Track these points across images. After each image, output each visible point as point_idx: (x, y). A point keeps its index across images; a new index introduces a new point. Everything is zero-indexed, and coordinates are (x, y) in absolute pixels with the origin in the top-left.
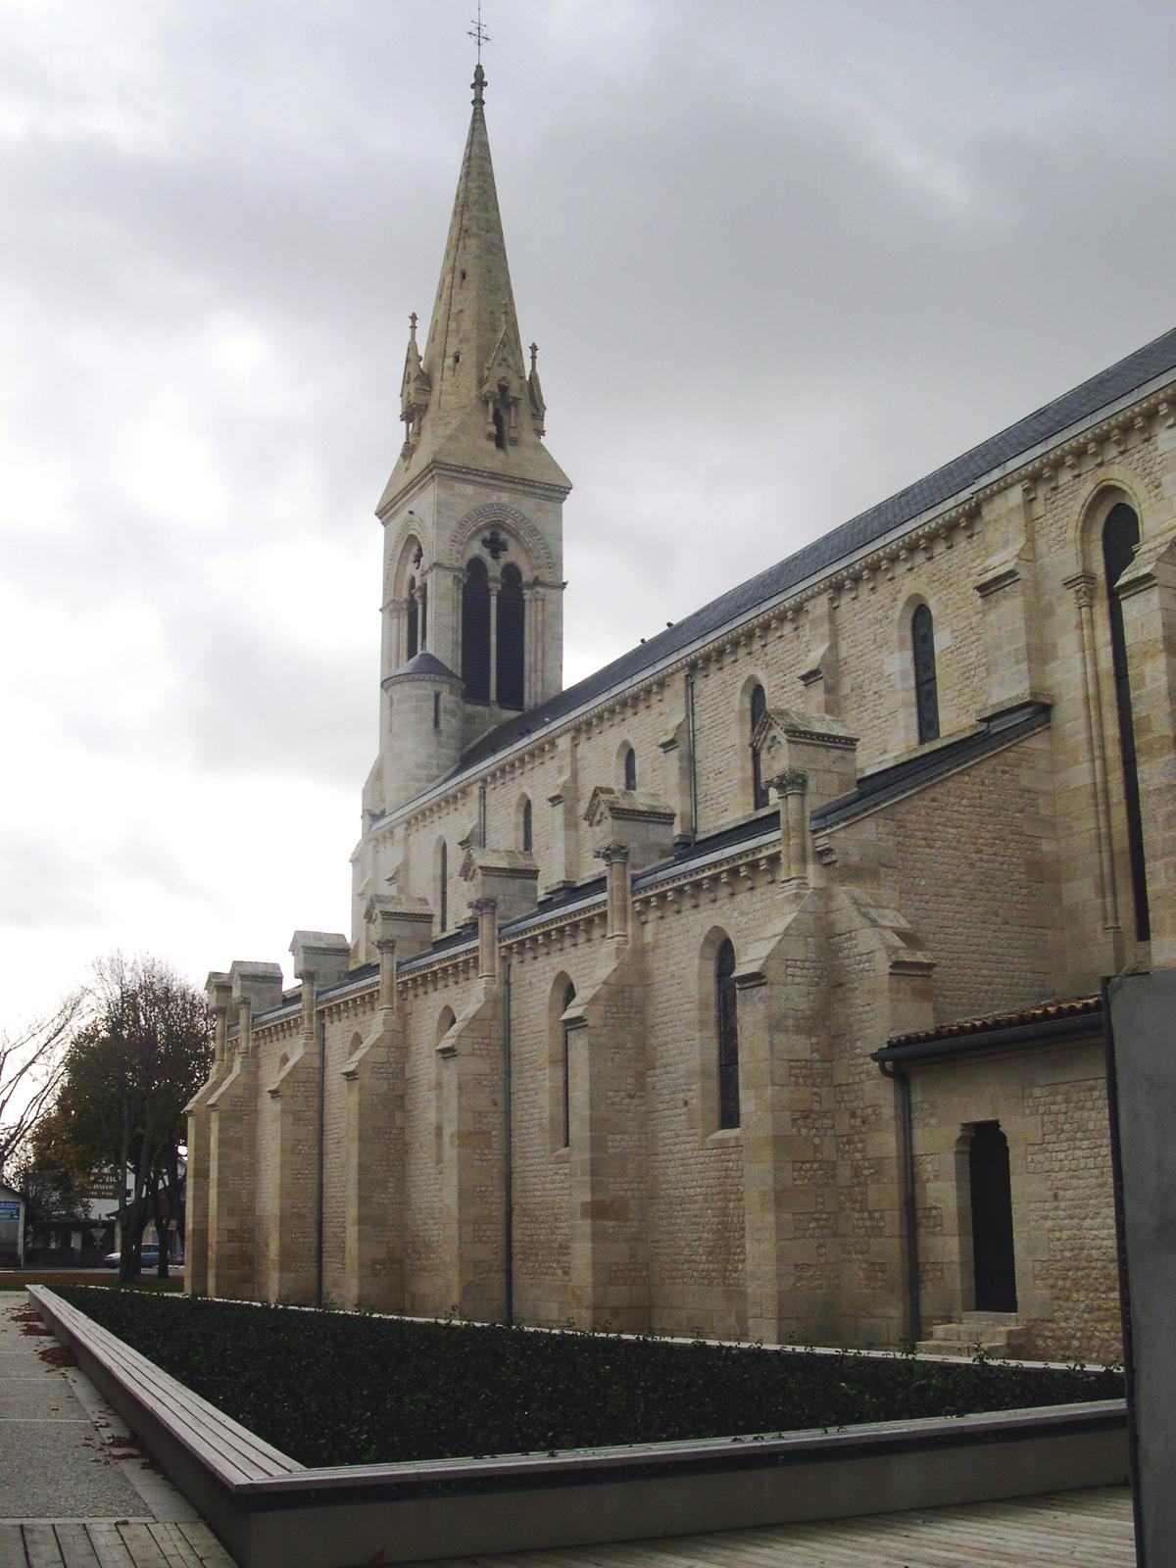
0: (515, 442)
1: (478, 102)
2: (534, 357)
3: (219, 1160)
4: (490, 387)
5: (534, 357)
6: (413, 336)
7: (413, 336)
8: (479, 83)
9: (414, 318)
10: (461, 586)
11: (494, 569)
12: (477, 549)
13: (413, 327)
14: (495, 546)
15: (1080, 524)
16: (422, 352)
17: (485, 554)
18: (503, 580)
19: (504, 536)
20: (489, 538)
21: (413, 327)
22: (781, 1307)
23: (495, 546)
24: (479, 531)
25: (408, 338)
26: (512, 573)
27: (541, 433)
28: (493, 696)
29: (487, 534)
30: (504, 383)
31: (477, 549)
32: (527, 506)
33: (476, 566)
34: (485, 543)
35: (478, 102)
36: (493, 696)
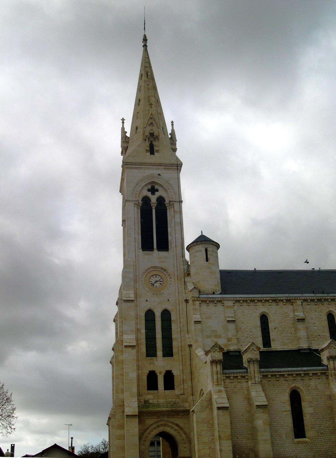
0: (158, 151)
1: (145, 46)
2: (172, 125)
3: (197, 436)
4: (147, 134)
5: (172, 125)
6: (123, 125)
7: (123, 125)
8: (145, 40)
9: (123, 120)
10: (139, 207)
11: (154, 199)
12: (146, 193)
13: (123, 123)
14: (153, 190)
15: (154, 436)
16: (128, 135)
17: (149, 194)
18: (157, 203)
19: (156, 187)
20: (150, 188)
21: (123, 123)
22: (268, 314)
23: (153, 190)
24: (146, 185)
25: (121, 126)
26: (161, 200)
27: (175, 150)
28: (155, 246)
29: (149, 187)
30: (152, 132)
31: (146, 193)
32: (166, 174)
33: (146, 200)
34: (149, 190)
35: (145, 46)
36: (155, 246)
